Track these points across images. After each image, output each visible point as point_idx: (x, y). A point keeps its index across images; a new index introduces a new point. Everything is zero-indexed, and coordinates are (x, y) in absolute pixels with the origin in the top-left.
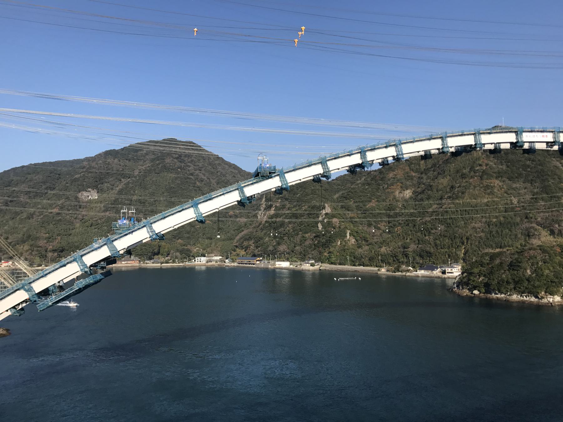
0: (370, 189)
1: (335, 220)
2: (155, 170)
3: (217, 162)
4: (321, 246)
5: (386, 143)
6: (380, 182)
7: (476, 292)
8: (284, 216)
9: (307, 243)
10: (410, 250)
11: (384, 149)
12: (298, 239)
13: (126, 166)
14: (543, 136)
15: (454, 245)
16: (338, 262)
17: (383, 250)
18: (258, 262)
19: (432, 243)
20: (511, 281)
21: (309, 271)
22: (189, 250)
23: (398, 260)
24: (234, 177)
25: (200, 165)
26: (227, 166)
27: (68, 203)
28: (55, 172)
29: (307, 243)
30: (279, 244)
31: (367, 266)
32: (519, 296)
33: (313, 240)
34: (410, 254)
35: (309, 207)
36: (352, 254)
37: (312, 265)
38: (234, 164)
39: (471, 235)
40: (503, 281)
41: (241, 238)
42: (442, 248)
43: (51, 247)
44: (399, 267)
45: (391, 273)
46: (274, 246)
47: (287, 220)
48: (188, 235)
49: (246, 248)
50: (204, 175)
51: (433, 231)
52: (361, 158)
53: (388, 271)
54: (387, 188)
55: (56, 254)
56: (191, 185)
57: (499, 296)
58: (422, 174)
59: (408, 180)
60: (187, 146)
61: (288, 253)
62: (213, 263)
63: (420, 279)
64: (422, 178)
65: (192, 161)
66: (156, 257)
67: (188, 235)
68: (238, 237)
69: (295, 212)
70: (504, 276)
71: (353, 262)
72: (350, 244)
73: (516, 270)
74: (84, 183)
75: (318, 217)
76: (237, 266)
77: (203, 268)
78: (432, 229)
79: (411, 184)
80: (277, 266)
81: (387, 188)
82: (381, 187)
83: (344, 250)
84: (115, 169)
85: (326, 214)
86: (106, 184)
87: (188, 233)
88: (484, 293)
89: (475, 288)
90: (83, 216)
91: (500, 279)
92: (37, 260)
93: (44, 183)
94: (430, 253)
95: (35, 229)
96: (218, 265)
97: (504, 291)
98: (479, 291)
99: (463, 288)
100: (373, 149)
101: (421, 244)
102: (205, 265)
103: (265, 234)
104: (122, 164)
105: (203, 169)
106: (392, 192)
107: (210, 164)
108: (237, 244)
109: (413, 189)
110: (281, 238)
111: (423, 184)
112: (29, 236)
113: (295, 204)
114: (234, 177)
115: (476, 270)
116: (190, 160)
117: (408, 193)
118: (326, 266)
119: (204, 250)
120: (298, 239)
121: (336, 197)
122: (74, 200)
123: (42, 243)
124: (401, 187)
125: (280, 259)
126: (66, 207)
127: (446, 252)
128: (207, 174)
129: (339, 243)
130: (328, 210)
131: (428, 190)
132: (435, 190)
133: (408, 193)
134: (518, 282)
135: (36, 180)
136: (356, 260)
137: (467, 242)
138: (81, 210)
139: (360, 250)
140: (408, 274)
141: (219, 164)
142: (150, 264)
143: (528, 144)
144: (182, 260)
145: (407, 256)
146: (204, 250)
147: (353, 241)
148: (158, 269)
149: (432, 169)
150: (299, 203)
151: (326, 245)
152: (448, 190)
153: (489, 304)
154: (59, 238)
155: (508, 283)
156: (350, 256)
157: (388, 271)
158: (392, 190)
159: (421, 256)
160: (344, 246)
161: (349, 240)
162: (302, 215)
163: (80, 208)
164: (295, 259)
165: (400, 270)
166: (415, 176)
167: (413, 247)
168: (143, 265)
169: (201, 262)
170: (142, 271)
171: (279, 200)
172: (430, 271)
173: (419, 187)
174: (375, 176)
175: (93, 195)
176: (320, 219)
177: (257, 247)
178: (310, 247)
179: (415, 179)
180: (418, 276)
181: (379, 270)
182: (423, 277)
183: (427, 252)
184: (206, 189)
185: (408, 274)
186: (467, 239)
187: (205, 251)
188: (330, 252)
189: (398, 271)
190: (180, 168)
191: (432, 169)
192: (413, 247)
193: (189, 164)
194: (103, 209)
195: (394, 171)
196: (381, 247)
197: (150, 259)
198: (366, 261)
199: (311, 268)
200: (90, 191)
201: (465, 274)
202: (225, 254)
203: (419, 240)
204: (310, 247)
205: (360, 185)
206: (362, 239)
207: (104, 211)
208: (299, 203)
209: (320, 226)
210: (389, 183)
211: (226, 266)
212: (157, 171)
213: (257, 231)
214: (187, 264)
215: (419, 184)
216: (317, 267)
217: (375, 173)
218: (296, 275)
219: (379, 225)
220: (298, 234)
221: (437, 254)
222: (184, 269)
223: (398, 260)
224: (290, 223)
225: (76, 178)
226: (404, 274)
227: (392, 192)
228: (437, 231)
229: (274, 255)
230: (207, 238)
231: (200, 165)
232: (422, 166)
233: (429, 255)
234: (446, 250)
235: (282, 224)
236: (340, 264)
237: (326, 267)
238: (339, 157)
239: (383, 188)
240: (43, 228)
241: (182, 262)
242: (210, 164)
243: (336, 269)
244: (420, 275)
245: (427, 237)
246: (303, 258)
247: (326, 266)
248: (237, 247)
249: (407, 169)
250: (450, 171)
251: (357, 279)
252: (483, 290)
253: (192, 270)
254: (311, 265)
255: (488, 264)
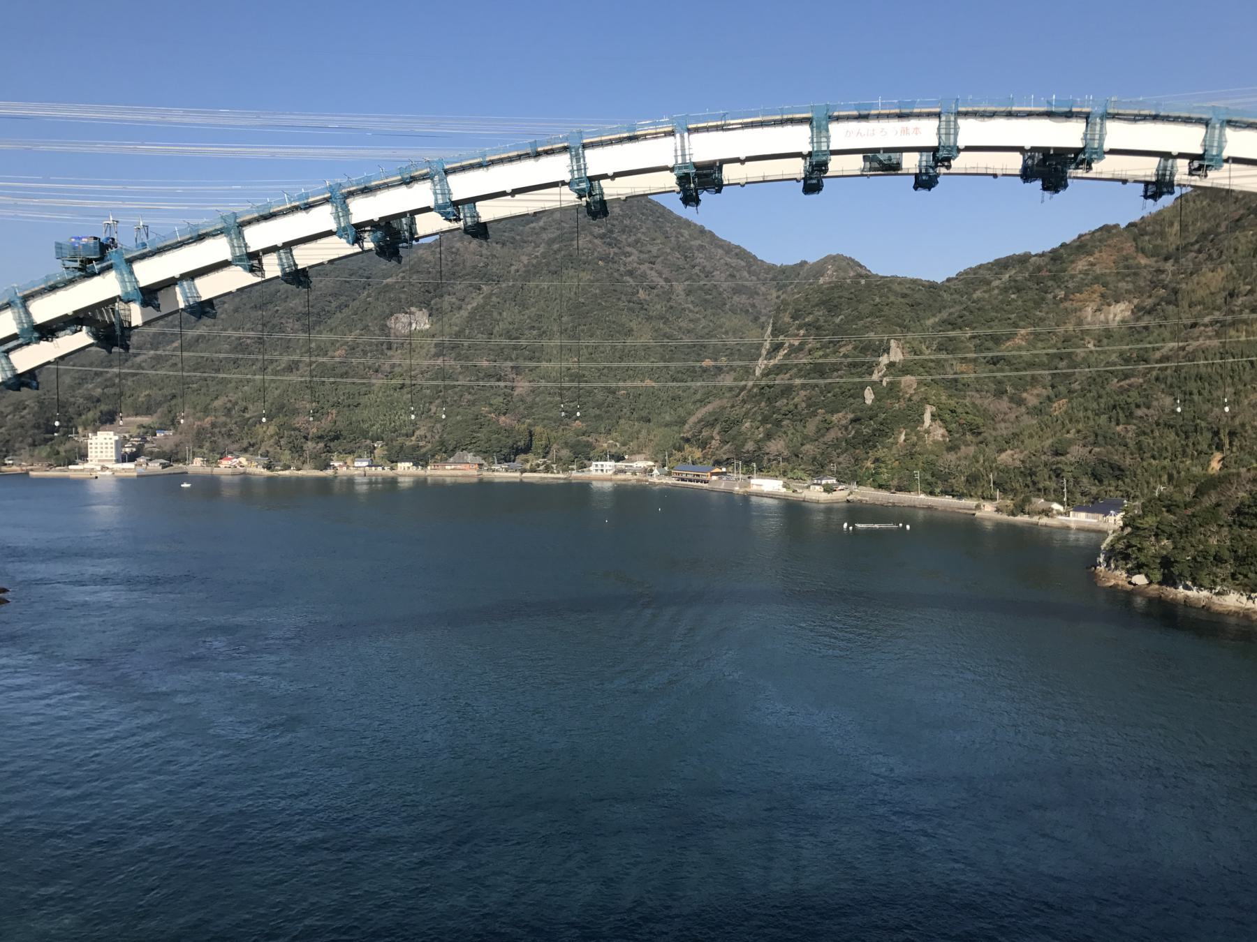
0: (1020, 303)
1: (908, 380)
2: (548, 264)
3: (696, 243)
4: (864, 441)
5: (401, 171)
6: (1050, 283)
7: (1140, 580)
8: (795, 370)
9: (831, 436)
10: (1070, 458)
11: (404, 189)
12: (811, 427)
13: (494, 256)
14: (905, 131)
15: (1189, 451)
16: (895, 482)
17: (1005, 457)
18: (714, 478)
19: (1131, 444)
20: (1226, 554)
21: (818, 502)
22: (589, 445)
23: (1034, 483)
24: (732, 276)
25: (654, 250)
26: (720, 251)
27: (365, 338)
28: (361, 272)
29: (831, 436)
30: (769, 436)
31: (961, 496)
32: (1245, 598)
33: (846, 429)
34: (1066, 469)
35: (855, 348)
36: (930, 467)
37: (829, 489)
38: (738, 247)
39: (1243, 425)
40: (1205, 553)
41: (699, 422)
42: (1154, 457)
43: (315, 430)
44: (1027, 500)
45: (1004, 517)
46: (757, 442)
47: (798, 381)
48: (598, 412)
49: (703, 445)
50: (660, 274)
51: (1139, 412)
52: (337, 218)
53: (998, 510)
54: (1066, 298)
55: (321, 445)
56: (624, 298)
57: (1193, 593)
58: (1166, 259)
59: (1124, 277)
60: (64, 197)
61: (786, 460)
62: (628, 475)
63: (1072, 537)
64: (1163, 272)
65: (637, 241)
66: (522, 457)
67: (598, 412)
68: (693, 420)
69: (820, 361)
70: (1213, 541)
71: (930, 484)
72: (929, 440)
73: (1247, 526)
74: (403, 296)
75: (871, 374)
76: (675, 486)
77: (608, 485)
78: (1138, 406)
79: (1130, 286)
80: (754, 488)
81: (1066, 298)
82: (1050, 296)
83: (912, 455)
84: (468, 264)
85: (891, 365)
86: (447, 298)
87: (599, 406)
88: (1160, 583)
89: (1139, 568)
90: (393, 366)
91: (1201, 547)
92: (286, 456)
93: (335, 295)
94: (1120, 469)
95: (294, 392)
96: (638, 480)
97: (1206, 582)
98: (1147, 576)
99: (1116, 568)
100: (367, 191)
101: (1100, 446)
102: (611, 480)
103: (746, 414)
104: (484, 252)
105: (659, 260)
106: (1076, 310)
107: (679, 247)
108: (689, 435)
109: (1136, 301)
110: (778, 423)
111: (1163, 287)
112: (282, 407)
113: (827, 339)
114: (732, 276)
115: (1150, 521)
116: (631, 240)
117: (1119, 312)
118: (866, 494)
119: (624, 444)
120: (811, 427)
121: (930, 322)
122: (377, 332)
123: (299, 421)
124: (1103, 296)
125: (763, 471)
126: (361, 347)
127: (1164, 468)
128: (666, 273)
129: (903, 437)
130: (896, 355)
131: (1168, 303)
132: (1185, 304)
133: (1119, 312)
134: (1244, 559)
135: (320, 289)
136: (937, 481)
137: (1231, 444)
138: (390, 353)
139: (951, 457)
140: (1044, 520)
141: (701, 248)
142: (501, 474)
143: (916, 155)
144: (565, 465)
145: (1058, 474)
146: (624, 444)
147: (939, 433)
148: (471, 484)
149: (1197, 247)
150: (836, 338)
151: (868, 442)
152: (1220, 301)
153: (1169, 616)
154: (334, 411)
155: (1219, 560)
156: (924, 470)
157: (998, 510)
158: (1075, 305)
159: (1097, 477)
160: (914, 445)
161: (928, 432)
162: (835, 368)
163: (390, 348)
164: (800, 474)
165: (1027, 509)
166: (1145, 267)
167: (1077, 452)
168: (487, 475)
169: (602, 472)
170: (484, 487)
171: (802, 332)
172: (1101, 516)
173: (1150, 296)
174: (1039, 269)
175: (422, 321)
176: (875, 377)
177: (724, 442)
178: (836, 447)
179: (1144, 273)
180: (1068, 528)
181: (978, 507)
182: (1080, 530)
183: (1112, 466)
184: (659, 307)
185: (1044, 520)
186: (1232, 434)
187: (624, 449)
188: (877, 460)
189: (1023, 512)
190: (605, 258)
191: (1197, 247)
192: (1077, 452)
193: (628, 249)
194: (433, 351)
195: (1091, 254)
196: (1001, 451)
197: (506, 459)
198: (959, 482)
199: (824, 496)
200: (411, 313)
201: (1129, 530)
202: (660, 456)
203: (1096, 436)
204: (836, 447)
205: (996, 291)
206: (965, 428)
207: (437, 355)
208: (836, 338)
209: (869, 396)
210: (1070, 285)
211: (652, 484)
212: (553, 268)
213: (733, 406)
214: (576, 475)
215: (1154, 284)
216: (841, 494)
217: (1041, 261)
218: (794, 510)
219: (1024, 395)
220: (814, 414)
221: (1139, 471)
222: (568, 486)
223: (1034, 483)
224: (803, 386)
225: (387, 285)
226: (1035, 519)
227: (1076, 310)
228: (1151, 411)
229: (756, 463)
230: (639, 420)
231: (654, 250)
232: (1171, 239)
233: (1117, 473)
234: (1166, 462)
235: (787, 391)
236: (900, 489)
237: (863, 495)
238: (272, 216)
239: (1055, 297)
240: (308, 391)
241: (564, 471)
242: (679, 247)
243: (884, 501)
244: (1073, 525)
245: (1119, 428)
246: (818, 469)
247: (866, 494)
248: (687, 440)
249: (1129, 247)
250: (1236, 250)
251: (904, 527)
252: (1158, 576)
253: (585, 487)
254: (825, 491)
255: (1186, 506)
